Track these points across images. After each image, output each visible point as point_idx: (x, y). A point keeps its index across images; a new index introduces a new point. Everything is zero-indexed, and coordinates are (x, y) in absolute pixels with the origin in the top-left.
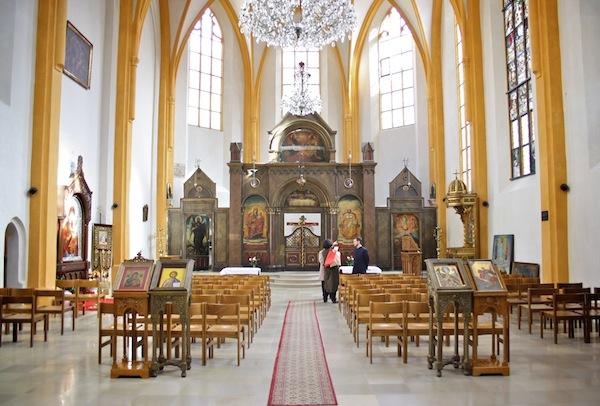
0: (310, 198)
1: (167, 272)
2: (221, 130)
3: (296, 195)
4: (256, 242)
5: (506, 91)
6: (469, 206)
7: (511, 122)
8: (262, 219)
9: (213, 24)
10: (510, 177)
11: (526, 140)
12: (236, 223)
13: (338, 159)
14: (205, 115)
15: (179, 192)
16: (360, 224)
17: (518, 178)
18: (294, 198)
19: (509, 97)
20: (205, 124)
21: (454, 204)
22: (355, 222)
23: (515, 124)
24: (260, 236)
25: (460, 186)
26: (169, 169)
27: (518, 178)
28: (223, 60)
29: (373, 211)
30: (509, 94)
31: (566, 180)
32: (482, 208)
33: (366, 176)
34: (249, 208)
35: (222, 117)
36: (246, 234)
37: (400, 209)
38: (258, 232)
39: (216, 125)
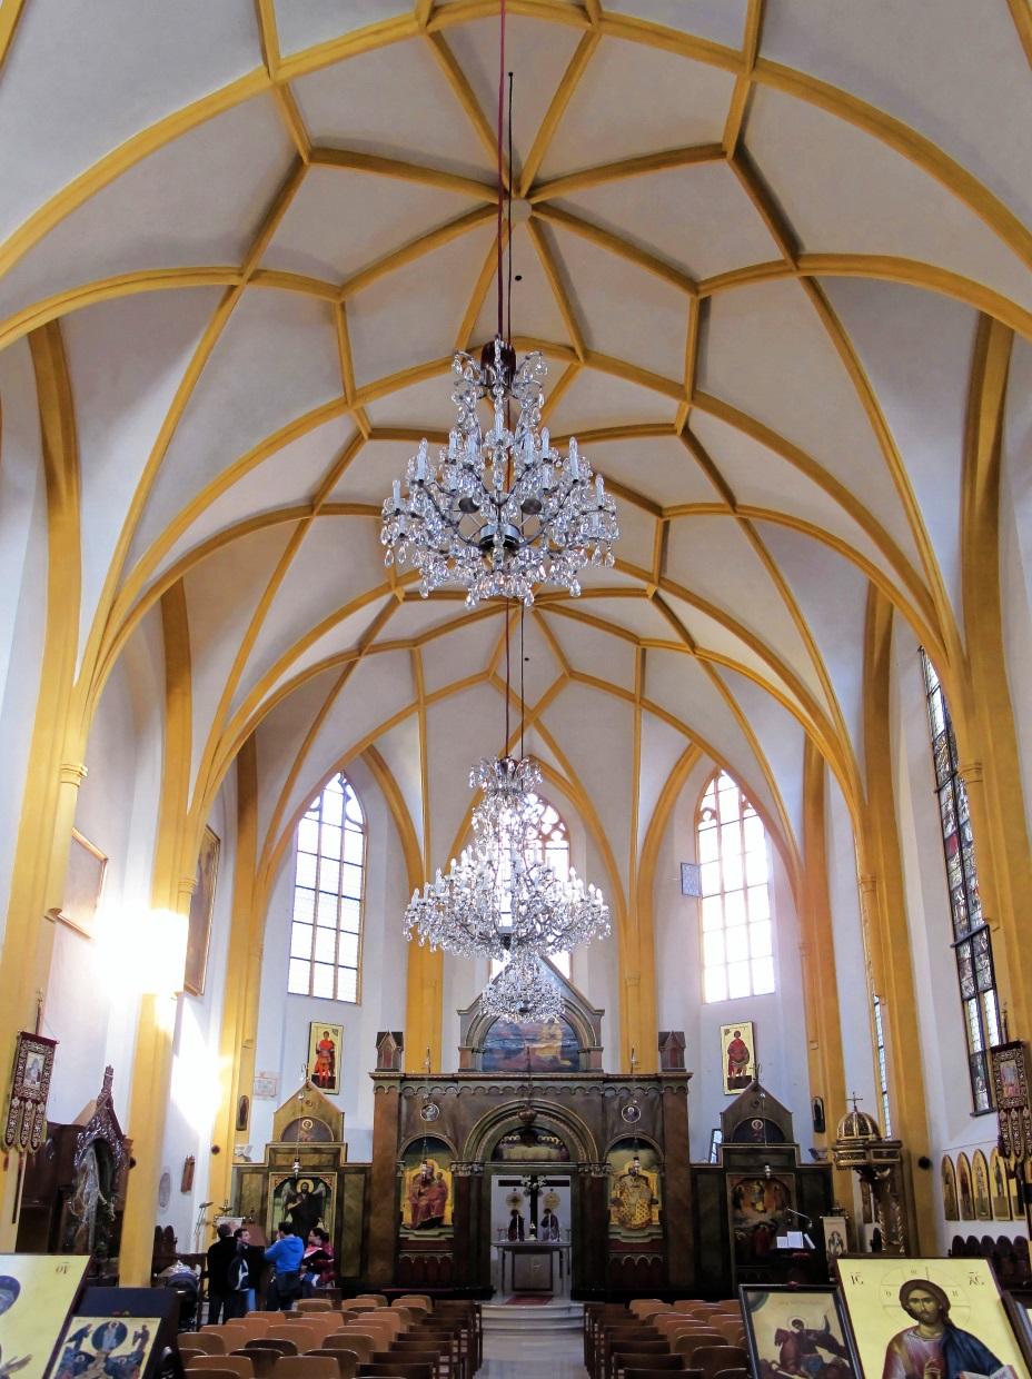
2: (358, 1003)
8: (442, 1185)
10: (971, 1110)
17: (986, 1112)
37: (744, 1169)
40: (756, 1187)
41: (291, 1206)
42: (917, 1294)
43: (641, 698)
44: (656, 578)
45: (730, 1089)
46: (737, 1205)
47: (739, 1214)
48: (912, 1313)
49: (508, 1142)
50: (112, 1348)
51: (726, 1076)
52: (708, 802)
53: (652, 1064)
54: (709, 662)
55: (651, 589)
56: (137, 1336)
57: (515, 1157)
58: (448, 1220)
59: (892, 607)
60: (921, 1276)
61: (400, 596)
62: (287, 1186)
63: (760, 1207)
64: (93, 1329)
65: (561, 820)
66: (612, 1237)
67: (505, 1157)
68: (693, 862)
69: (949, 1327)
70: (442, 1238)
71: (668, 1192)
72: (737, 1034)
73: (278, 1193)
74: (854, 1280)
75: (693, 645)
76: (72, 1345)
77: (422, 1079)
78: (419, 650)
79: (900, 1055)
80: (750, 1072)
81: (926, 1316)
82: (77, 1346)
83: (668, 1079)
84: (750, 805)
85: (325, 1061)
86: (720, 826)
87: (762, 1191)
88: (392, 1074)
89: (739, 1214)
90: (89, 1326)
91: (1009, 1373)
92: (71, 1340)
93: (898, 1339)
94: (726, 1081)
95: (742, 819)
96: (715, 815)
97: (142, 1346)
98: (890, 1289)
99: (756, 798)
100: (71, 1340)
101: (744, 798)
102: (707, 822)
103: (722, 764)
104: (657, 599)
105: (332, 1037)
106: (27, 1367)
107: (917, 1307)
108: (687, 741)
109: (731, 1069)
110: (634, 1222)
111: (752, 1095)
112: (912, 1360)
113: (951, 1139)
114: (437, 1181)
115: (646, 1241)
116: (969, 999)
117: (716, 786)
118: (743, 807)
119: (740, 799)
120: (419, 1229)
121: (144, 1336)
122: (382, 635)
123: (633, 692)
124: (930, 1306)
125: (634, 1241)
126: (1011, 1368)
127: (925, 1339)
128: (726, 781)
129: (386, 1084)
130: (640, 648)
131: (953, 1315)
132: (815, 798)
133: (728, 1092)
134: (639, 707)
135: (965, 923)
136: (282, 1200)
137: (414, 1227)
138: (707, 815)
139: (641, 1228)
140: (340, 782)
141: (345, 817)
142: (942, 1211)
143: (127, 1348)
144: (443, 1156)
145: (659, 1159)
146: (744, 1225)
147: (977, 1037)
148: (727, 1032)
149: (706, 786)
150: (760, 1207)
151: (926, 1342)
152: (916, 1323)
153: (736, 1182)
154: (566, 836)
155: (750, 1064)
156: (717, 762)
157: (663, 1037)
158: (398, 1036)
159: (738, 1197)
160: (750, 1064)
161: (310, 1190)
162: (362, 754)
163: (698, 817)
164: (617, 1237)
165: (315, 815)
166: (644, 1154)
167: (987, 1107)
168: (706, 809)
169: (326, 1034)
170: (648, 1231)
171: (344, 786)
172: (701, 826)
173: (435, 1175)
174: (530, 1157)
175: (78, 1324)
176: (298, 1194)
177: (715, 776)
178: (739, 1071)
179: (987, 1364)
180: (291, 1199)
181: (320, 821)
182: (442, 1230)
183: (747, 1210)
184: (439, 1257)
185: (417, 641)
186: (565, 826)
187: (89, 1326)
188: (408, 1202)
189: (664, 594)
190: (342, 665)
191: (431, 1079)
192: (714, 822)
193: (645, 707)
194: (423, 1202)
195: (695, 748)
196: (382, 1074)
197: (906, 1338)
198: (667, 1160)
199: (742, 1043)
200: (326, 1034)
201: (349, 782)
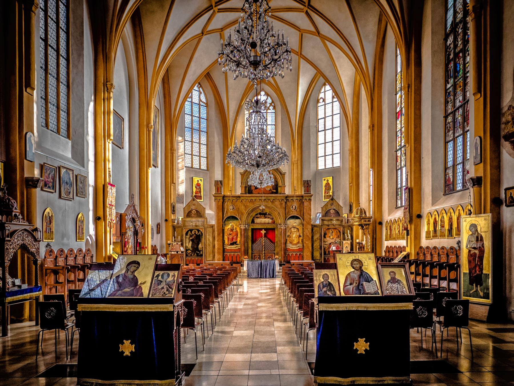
0: (269, 218)
1: (332, 255)
2: (207, 170)
3: (259, 216)
4: (233, 247)
5: (443, 115)
6: (367, 225)
7: (446, 143)
8: (237, 232)
9: (201, 93)
10: (395, 206)
11: (460, 160)
12: (219, 234)
13: (288, 191)
14: (196, 159)
15: (265, 330)
16: (302, 235)
17: (399, 207)
18: (258, 218)
19: (446, 120)
20: (196, 165)
21: (357, 223)
22: (298, 234)
23: (450, 145)
24: (235, 243)
25: (361, 212)
26: (173, 199)
27: (399, 207)
28: (207, 145)
29: (310, 227)
30: (446, 117)
31: (421, 212)
32: (378, 227)
33: (306, 204)
34: (228, 224)
35: (207, 148)
36: (226, 241)
37: (328, 225)
38: (234, 241)
39: (204, 167)
40: (331, 231)
41: (191, 238)
42: (355, 262)
43: (301, 54)
44: (307, 4)
45: (324, 199)
46: (325, 237)
47: (325, 240)
48: (353, 268)
49: (256, 217)
50: (166, 279)
51: (323, 195)
52: (322, 95)
53: (300, 191)
54: (324, 38)
55: (306, 9)
56: (172, 276)
57: (258, 222)
58: (238, 243)
59: (387, 22)
60: (357, 258)
61: (216, 11)
62: (189, 232)
63: (331, 237)
64: (161, 274)
65: (273, 102)
66: (288, 247)
67: (255, 222)
68: (249, 362)
69: (362, 271)
70: (237, 248)
71: (304, 233)
72: (328, 180)
73: (187, 234)
74: (340, 259)
75: (319, 33)
76: (156, 278)
77: (230, 197)
78: (223, 33)
79: (376, 189)
80: (331, 194)
81: (357, 268)
82: (157, 278)
83: (305, 196)
84: (335, 97)
85: (198, 190)
86: (325, 105)
87: (332, 232)
88: (220, 195)
89: (325, 240)
90: (160, 273)
91: (375, 282)
92: (155, 277)
93: (349, 274)
94: (323, 197)
95: (333, 102)
96: (324, 100)
97: (174, 278)
98: (348, 261)
99: (337, 94)
100: (155, 277)
101: (334, 94)
102: (321, 103)
103: (327, 81)
104: (307, 13)
105: (200, 182)
106: (145, 284)
107: (354, 266)
108: (316, 71)
109: (325, 192)
110: (294, 243)
111: (331, 201)
112: (351, 279)
113: (389, 215)
114: (235, 230)
115: (298, 248)
116: (398, 170)
117: (325, 89)
118: (333, 97)
119: (332, 94)
120: (230, 245)
121: (174, 276)
122: (210, 28)
123: (297, 51)
124: (358, 266)
125: (294, 248)
126: (375, 281)
127: (356, 274)
128: (328, 87)
129: (218, 198)
130: (301, 33)
131: (363, 268)
132: (357, 96)
133: (324, 200)
134: (300, 57)
135: (400, 143)
136: (188, 237)
137: (228, 245)
138: (321, 100)
139: (296, 244)
140: (197, 86)
141: (200, 100)
142: (384, 237)
143: (170, 279)
144: (235, 221)
145: (302, 222)
146: (326, 243)
147: (399, 183)
148: (325, 180)
149: (322, 87)
150: (331, 237)
151: (356, 275)
152: (354, 270)
153: (325, 230)
154: (274, 108)
155: (331, 191)
156: (326, 80)
157: (305, 181)
158: (221, 182)
159: (325, 234)
160: (331, 191)
161: (197, 233)
162: (205, 76)
163: (318, 101)
164: (289, 247)
165: (189, 100)
166: (297, 221)
167: (400, 206)
168: (321, 98)
169: (198, 181)
170: (298, 245)
171: (199, 88)
172: (319, 105)
173: (234, 228)
174: (263, 222)
175: (157, 273)
176: (193, 235)
177: (325, 85)
178: (328, 193)
179: (370, 280)
180: (191, 236)
181: (191, 102)
182: (236, 246)
183: (328, 239)
184: (236, 254)
185: (222, 29)
186: (274, 104)
187: (160, 273)
188: (226, 237)
189: (309, 11)
190: (196, 40)
191: (232, 197)
192: (323, 103)
193: (302, 57)
194: (231, 237)
195: (318, 74)
196: (217, 195)
197: (351, 274)
198: (305, 223)
199: (329, 184)
200: (198, 181)
201: (201, 86)
